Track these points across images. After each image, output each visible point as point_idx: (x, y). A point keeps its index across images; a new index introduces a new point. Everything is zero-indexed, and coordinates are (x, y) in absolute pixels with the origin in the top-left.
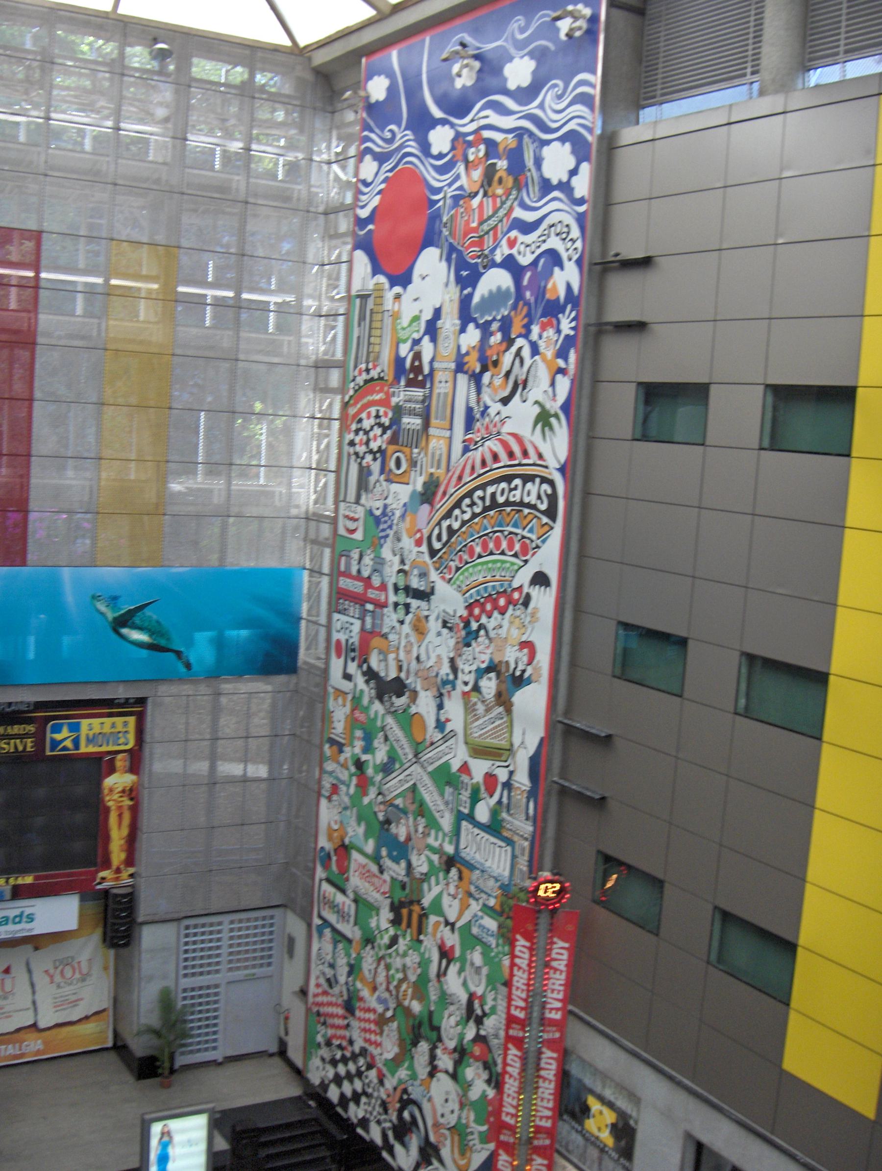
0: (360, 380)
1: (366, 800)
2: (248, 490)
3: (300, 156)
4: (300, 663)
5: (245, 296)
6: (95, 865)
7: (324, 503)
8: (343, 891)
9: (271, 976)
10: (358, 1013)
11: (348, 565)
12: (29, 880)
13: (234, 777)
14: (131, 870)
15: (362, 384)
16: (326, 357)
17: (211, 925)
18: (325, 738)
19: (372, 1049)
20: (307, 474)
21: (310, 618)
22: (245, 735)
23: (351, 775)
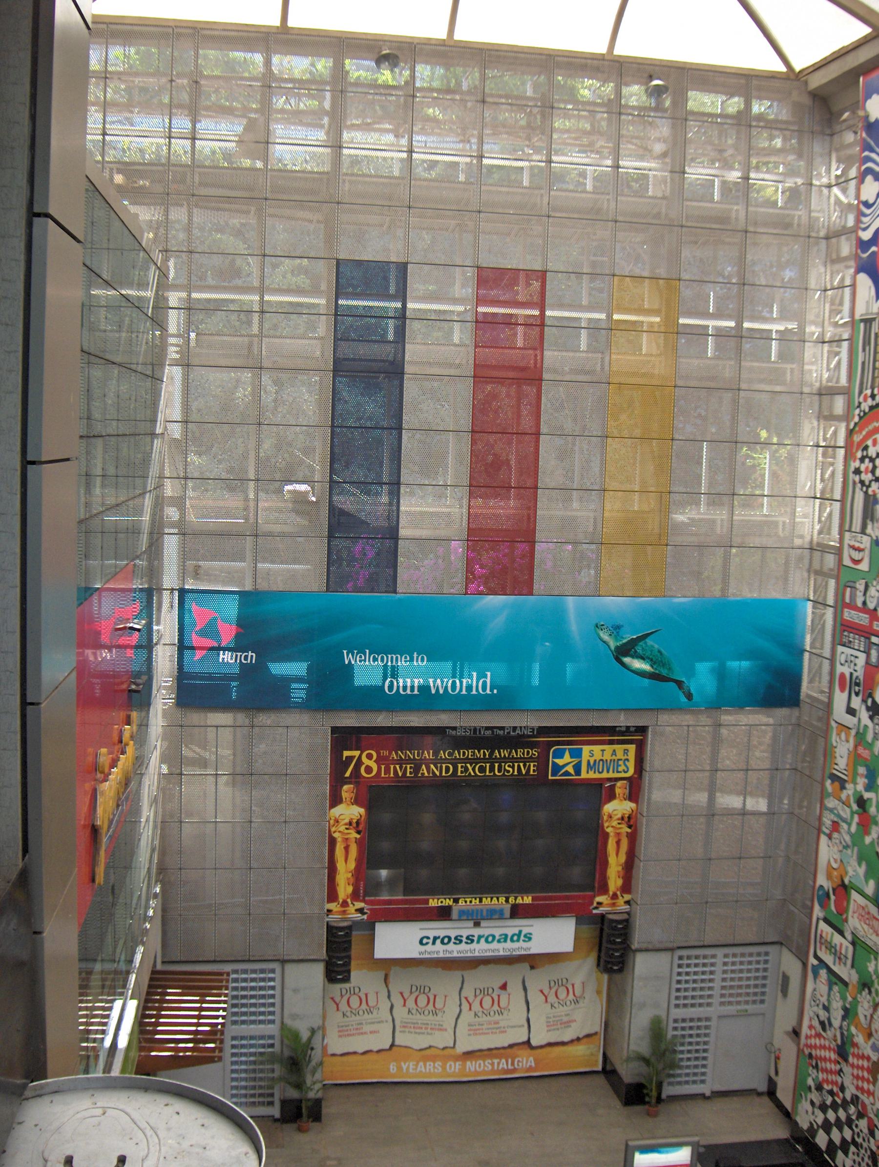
0: (865, 407)
1: (868, 840)
2: (750, 521)
3: (800, 181)
4: (802, 696)
5: (746, 325)
6: (592, 888)
7: (829, 533)
8: (841, 933)
9: (763, 1014)
10: (851, 1059)
11: (853, 597)
12: (528, 900)
13: (733, 809)
14: (627, 897)
15: (867, 410)
16: (830, 384)
17: (705, 957)
18: (827, 774)
19: (863, 1097)
20: (812, 504)
21: (814, 651)
22: (745, 767)
23: (853, 813)
